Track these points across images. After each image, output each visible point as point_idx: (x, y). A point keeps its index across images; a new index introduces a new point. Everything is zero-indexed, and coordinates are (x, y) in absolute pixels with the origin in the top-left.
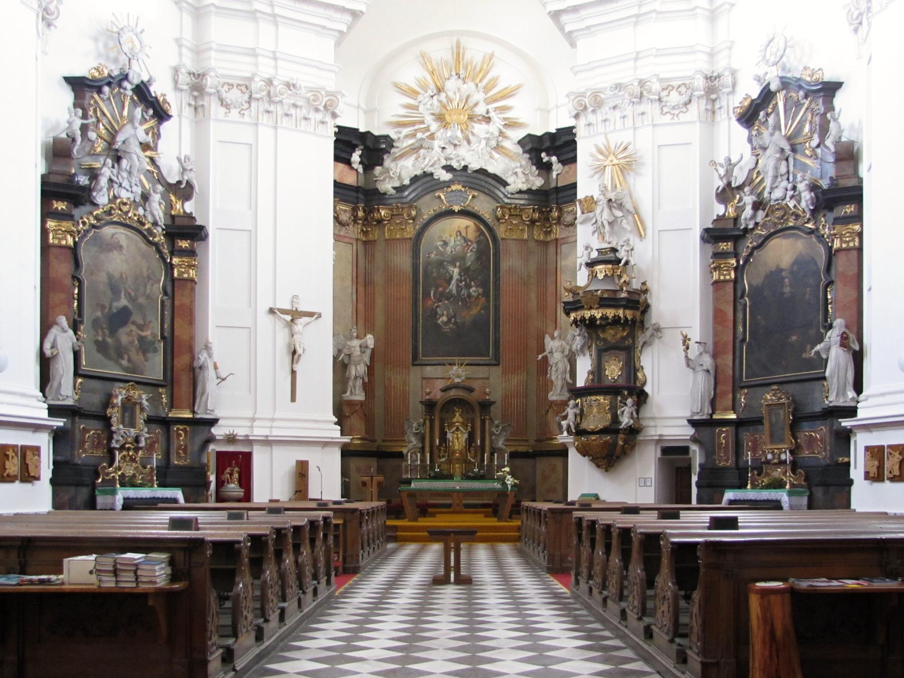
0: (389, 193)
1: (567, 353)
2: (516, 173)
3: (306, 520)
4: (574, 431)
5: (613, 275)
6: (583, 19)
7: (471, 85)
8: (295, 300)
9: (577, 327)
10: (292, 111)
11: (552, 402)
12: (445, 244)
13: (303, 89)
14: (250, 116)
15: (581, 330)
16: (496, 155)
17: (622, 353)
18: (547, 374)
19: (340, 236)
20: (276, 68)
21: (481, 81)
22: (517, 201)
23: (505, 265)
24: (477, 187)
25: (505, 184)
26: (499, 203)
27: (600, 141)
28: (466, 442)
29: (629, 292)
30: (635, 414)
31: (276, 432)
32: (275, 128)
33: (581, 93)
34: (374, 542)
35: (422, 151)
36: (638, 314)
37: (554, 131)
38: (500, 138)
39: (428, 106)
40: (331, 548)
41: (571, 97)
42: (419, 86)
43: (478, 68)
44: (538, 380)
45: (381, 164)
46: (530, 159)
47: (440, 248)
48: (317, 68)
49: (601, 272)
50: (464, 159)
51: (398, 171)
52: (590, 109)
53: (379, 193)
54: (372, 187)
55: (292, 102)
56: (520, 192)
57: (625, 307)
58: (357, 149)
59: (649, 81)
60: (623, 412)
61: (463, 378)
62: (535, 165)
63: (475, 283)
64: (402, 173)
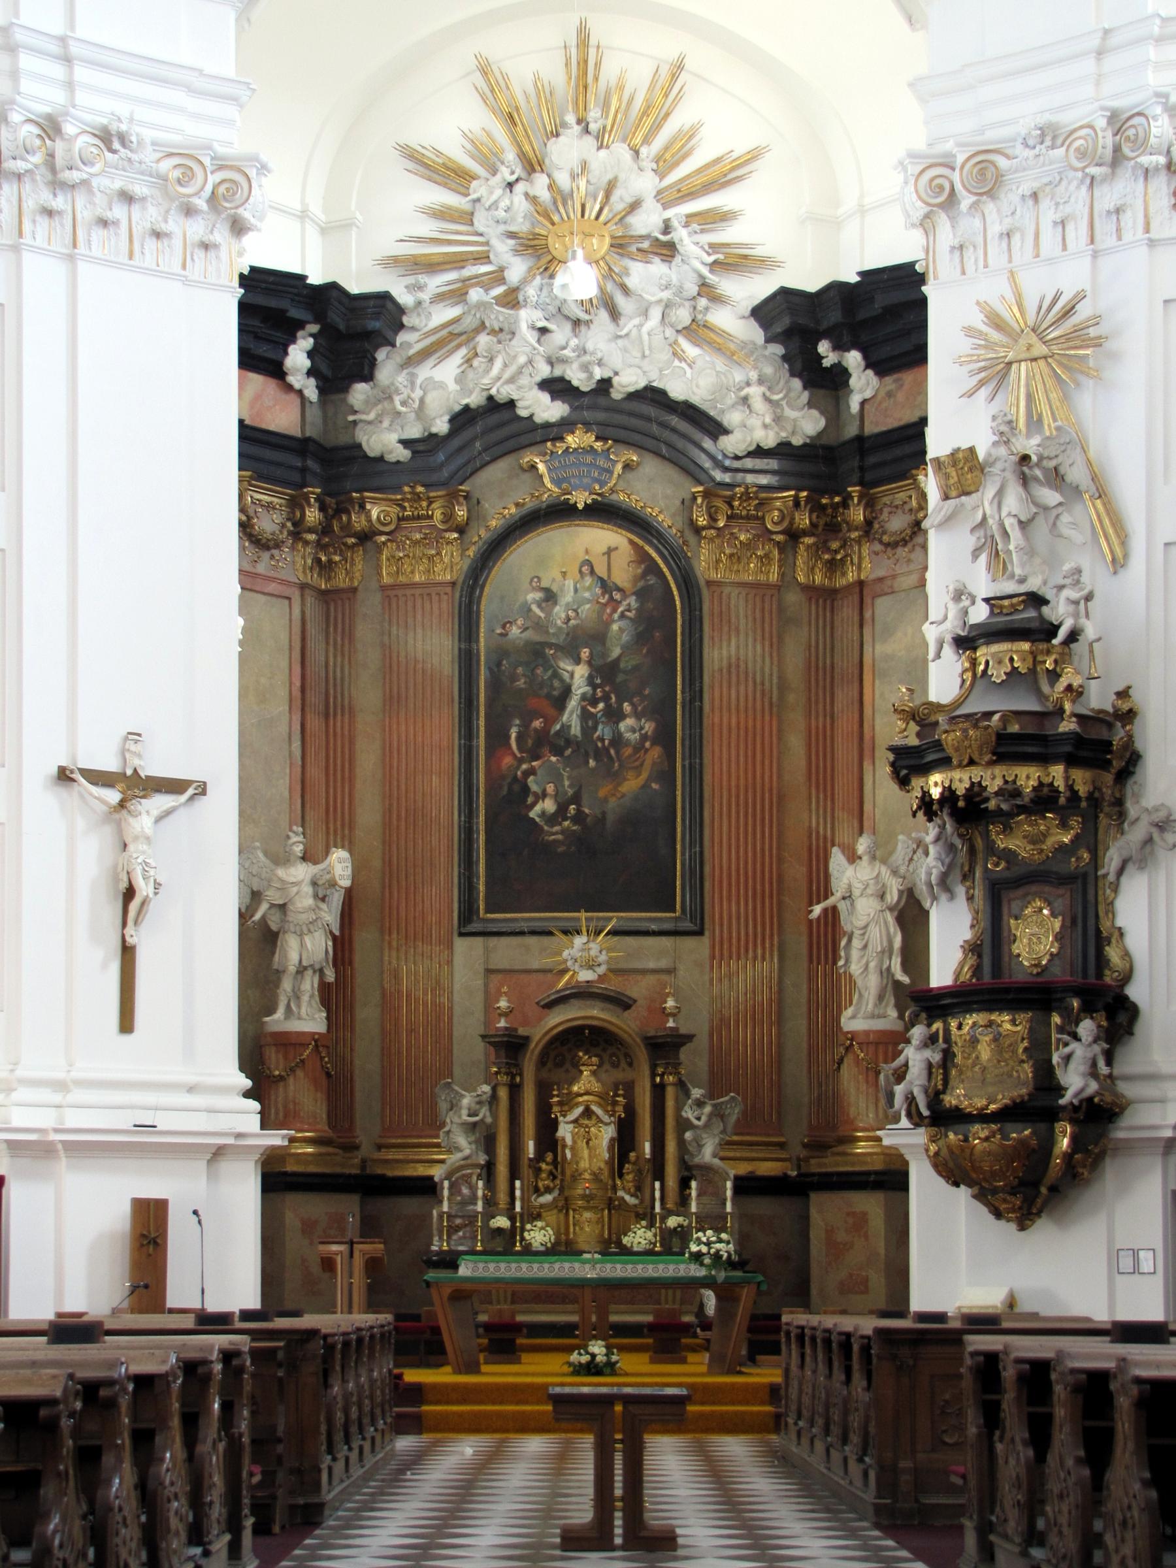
0: (392, 458)
1: (893, 897)
2: (745, 400)
3: (173, 1359)
4: (925, 1112)
5: (1033, 671)
7: (621, 151)
9: (930, 820)
10: (119, 212)
11: (853, 1036)
12: (550, 597)
13: (150, 148)
16: (691, 351)
17: (1061, 891)
18: (836, 958)
19: (256, 575)
20: (70, 85)
21: (647, 141)
22: (750, 478)
23: (715, 655)
24: (637, 437)
25: (716, 429)
26: (700, 483)
28: (611, 1148)
29: (1081, 718)
31: (74, 1119)
34: (361, 1430)
35: (483, 340)
36: (1108, 778)
37: (854, 279)
38: (703, 302)
39: (501, 214)
40: (241, 1444)
42: (473, 157)
43: (639, 103)
45: (368, 377)
46: (785, 358)
47: (534, 608)
48: (191, 90)
50: (600, 363)
51: (417, 394)
53: (366, 456)
54: (343, 439)
55: (118, 184)
56: (759, 452)
57: (1071, 761)
58: (300, 334)
60: (1068, 1058)
61: (601, 970)
62: (799, 375)
63: (632, 704)
64: (429, 399)
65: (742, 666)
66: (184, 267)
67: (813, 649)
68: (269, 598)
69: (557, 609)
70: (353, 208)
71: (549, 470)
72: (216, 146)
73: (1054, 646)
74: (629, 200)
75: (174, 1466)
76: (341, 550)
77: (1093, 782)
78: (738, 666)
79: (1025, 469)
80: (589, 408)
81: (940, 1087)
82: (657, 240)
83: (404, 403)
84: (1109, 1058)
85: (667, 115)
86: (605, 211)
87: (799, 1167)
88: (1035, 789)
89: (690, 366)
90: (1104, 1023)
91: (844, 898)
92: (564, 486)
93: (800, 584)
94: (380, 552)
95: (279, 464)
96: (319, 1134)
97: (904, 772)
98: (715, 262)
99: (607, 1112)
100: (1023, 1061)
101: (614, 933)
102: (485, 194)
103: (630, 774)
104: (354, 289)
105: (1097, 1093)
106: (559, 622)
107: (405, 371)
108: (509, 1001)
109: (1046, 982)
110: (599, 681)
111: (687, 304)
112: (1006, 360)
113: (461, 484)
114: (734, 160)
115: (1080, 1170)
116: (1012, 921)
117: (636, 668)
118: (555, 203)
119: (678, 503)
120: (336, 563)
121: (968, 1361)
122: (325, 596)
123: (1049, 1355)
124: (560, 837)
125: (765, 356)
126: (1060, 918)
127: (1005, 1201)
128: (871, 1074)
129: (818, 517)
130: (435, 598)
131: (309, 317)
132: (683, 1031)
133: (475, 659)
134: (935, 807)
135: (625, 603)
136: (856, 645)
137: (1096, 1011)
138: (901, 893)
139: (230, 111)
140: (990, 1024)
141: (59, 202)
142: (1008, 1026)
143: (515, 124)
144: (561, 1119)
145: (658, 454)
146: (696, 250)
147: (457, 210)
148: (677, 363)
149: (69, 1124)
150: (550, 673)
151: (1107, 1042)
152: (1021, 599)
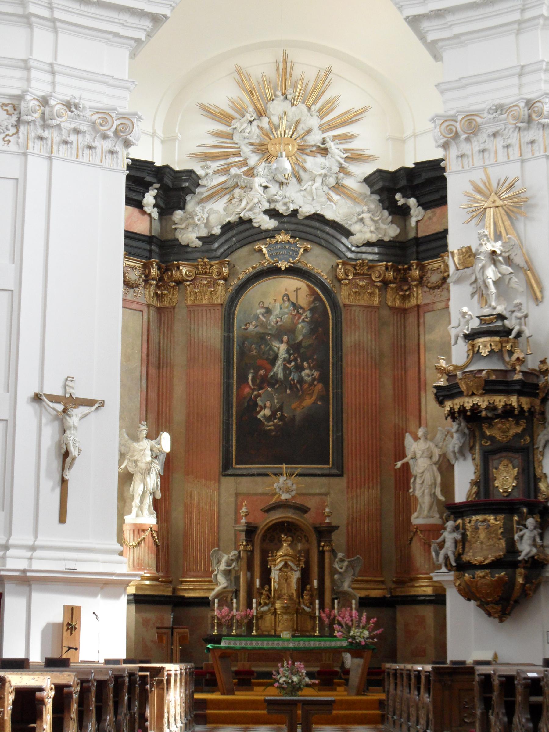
1: (436, 458)
2: (362, 220)
4: (454, 564)
5: (501, 350)
6: (451, 26)
7: (304, 108)
8: (68, 383)
9: (454, 421)
10: (73, 138)
11: (418, 527)
13: (88, 110)
14: (18, 143)
15: (460, 424)
16: (336, 197)
17: (517, 456)
18: (408, 488)
20: (53, 84)
21: (314, 103)
22: (364, 256)
25: (348, 233)
26: (340, 258)
27: (478, 176)
29: (524, 373)
30: (538, 539)
31: (37, 565)
32: (50, 158)
33: (452, 116)
35: (237, 191)
36: (538, 401)
37: (412, 166)
38: (341, 175)
41: (437, 122)
42: (233, 109)
43: (311, 86)
44: (397, 497)
45: (183, 208)
46: (380, 201)
47: (261, 316)
49: (485, 346)
50: (293, 202)
52: (463, 136)
53: (180, 244)
54: (170, 237)
55: (73, 126)
56: (368, 244)
57: (520, 393)
58: (150, 188)
59: (538, 101)
60: (521, 537)
61: (294, 493)
62: (387, 209)
63: (308, 363)
64: (211, 218)
65: (361, 345)
66: (101, 162)
67: (395, 337)
68: (132, 311)
69: (272, 317)
70: (177, 131)
71: (268, 251)
72: (118, 109)
73: (510, 339)
74: (306, 129)
75: (110, 723)
76: (167, 288)
77: (531, 403)
78: (359, 345)
79: (494, 257)
80: (287, 223)
81: (461, 552)
82: (319, 147)
83: (199, 220)
84: (542, 538)
85: (324, 92)
86: (295, 134)
87: (391, 593)
88: (503, 407)
89: (335, 204)
90: (539, 520)
91: (412, 458)
92: (275, 259)
93: (388, 306)
94: (186, 289)
95: (139, 248)
96: (152, 575)
97: (441, 398)
98: (347, 157)
99: (296, 565)
100: (500, 539)
101: (300, 475)
102: (239, 126)
103: (307, 397)
104: (177, 168)
105: (536, 554)
106: (273, 324)
107: (200, 206)
108: (247, 509)
109: (510, 500)
110: (292, 352)
111: (334, 176)
112: (484, 207)
113: (226, 258)
114: (355, 112)
115: (529, 592)
116: (494, 470)
117: (310, 346)
118: (271, 130)
119: (330, 267)
120: (165, 294)
121: (477, 678)
122: (159, 310)
123: (514, 673)
124: (273, 427)
125: (371, 200)
126: (517, 469)
127: (493, 608)
128: (427, 546)
129: (397, 275)
130: (212, 311)
131: (155, 181)
132: (333, 524)
133: (231, 340)
134: (456, 415)
135: (304, 314)
136: (416, 335)
137: (535, 514)
138: (440, 456)
139: (126, 94)
140: (484, 521)
141: (46, 134)
142: (492, 521)
143: (253, 95)
144: (273, 568)
145: (320, 245)
146: (337, 152)
147: (226, 133)
148: (329, 202)
149: (34, 567)
150: (268, 348)
151: (541, 529)
152: (495, 316)
